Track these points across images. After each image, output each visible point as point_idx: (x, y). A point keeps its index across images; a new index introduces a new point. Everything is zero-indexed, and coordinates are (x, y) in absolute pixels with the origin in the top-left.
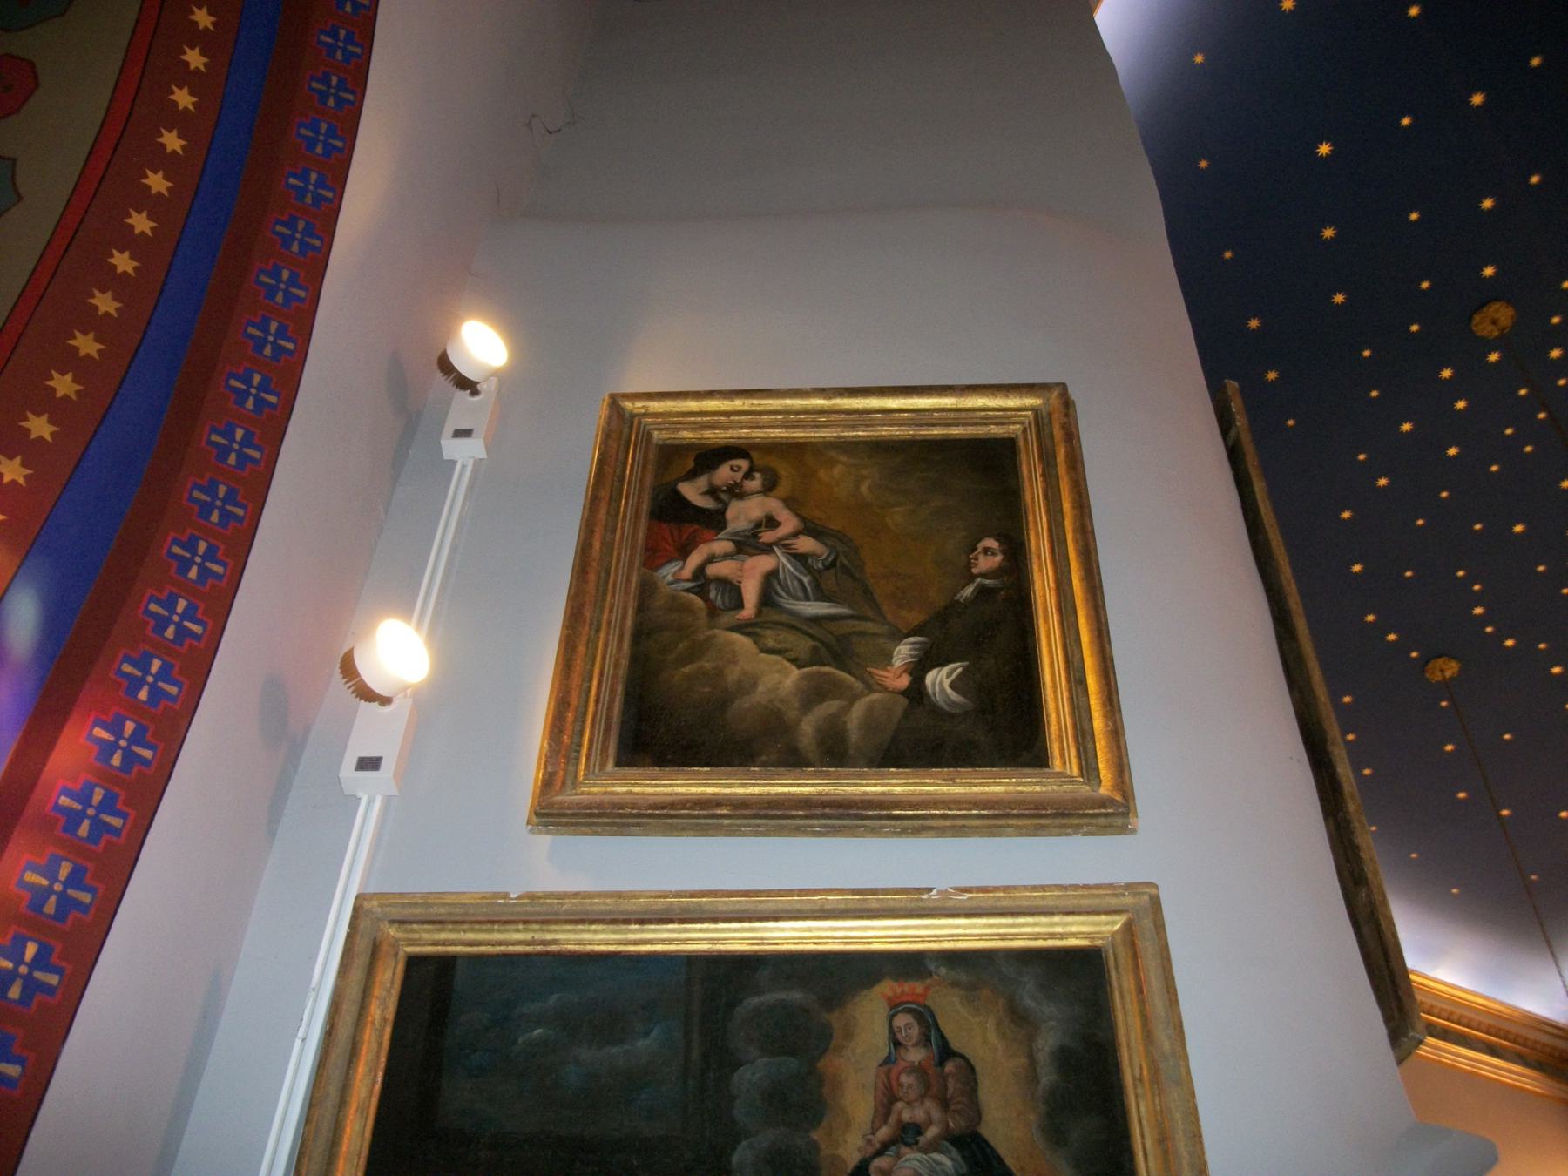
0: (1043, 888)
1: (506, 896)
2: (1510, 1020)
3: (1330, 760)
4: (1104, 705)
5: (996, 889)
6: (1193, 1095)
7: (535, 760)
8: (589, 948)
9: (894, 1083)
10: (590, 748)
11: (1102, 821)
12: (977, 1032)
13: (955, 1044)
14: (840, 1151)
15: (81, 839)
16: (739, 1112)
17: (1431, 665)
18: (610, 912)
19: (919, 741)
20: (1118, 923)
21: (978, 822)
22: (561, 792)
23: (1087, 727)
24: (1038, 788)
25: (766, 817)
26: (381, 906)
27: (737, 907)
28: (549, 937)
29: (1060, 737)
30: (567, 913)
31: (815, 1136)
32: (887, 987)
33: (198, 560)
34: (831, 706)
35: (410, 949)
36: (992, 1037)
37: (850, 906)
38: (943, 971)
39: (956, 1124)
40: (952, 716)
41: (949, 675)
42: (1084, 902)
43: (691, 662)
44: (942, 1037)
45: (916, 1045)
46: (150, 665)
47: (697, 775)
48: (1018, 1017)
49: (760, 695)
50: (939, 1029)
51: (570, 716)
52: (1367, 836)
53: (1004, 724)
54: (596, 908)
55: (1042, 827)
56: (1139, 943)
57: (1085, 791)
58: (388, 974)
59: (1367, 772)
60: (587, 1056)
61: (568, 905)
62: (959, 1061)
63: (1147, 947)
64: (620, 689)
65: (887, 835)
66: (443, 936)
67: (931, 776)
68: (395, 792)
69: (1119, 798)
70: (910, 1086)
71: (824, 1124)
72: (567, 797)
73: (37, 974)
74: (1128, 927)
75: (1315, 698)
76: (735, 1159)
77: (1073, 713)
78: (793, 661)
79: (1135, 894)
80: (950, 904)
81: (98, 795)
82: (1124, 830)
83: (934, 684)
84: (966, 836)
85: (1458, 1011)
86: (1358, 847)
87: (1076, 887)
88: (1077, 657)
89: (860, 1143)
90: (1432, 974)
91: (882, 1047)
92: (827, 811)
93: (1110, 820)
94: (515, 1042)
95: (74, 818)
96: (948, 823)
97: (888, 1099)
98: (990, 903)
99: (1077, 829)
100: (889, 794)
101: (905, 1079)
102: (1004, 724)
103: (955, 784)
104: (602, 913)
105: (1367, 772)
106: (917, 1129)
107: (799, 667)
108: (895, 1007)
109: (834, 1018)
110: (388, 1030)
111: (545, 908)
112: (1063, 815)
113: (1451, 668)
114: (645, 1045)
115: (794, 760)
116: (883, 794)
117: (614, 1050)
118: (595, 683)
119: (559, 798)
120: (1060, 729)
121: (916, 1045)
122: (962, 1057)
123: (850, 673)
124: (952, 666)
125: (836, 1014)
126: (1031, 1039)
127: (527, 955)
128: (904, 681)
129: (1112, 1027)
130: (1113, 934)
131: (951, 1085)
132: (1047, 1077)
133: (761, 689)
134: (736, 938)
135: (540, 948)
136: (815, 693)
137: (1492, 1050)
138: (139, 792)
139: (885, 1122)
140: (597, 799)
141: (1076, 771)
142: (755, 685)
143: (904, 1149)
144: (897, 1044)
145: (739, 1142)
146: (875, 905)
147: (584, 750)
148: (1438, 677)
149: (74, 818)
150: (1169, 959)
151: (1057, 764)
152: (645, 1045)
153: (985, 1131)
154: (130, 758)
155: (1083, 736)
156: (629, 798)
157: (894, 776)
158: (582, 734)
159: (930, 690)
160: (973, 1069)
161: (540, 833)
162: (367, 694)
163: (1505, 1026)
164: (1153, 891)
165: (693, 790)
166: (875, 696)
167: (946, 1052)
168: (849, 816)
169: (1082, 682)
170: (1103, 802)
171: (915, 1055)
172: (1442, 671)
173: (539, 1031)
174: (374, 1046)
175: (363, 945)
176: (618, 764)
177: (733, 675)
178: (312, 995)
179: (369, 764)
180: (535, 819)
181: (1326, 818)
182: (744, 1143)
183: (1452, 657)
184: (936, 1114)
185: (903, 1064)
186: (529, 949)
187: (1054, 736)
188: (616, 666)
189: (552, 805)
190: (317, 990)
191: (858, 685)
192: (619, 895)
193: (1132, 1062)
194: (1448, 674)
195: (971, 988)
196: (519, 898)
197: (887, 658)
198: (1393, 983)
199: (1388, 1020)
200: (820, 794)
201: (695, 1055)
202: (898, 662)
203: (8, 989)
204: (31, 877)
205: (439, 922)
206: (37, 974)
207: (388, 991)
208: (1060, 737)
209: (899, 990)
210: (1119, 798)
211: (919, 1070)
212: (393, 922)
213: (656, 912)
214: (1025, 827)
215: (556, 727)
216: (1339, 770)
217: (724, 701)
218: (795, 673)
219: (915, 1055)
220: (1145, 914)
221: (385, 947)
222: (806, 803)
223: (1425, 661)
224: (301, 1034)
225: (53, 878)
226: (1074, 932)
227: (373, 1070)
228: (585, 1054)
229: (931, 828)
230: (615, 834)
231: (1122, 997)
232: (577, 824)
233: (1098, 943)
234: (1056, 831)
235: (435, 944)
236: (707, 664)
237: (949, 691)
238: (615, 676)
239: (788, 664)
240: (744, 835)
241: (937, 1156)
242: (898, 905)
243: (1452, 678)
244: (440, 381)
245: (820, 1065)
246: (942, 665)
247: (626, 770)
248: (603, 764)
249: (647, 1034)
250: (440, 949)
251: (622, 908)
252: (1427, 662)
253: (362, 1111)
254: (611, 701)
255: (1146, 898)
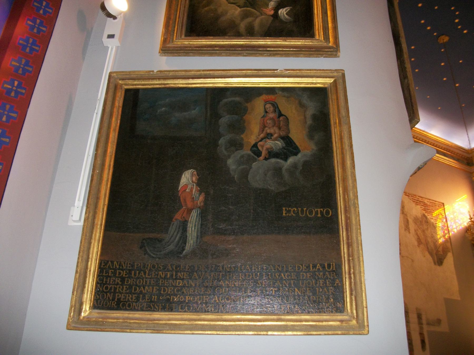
0: (310, 70)
1: (153, 71)
2: (451, 147)
3: (400, 43)
4: (332, 20)
5: (297, 70)
6: (350, 127)
7: (161, 34)
8: (177, 86)
9: (265, 123)
10: (177, 31)
11: (329, 53)
12: (289, 109)
13: (283, 113)
14: (249, 140)
15: (4, 122)
16: (221, 130)
17: (440, 38)
18: (183, 76)
19: (276, 29)
20: (332, 80)
21: (293, 53)
22: (168, 44)
23: (326, 26)
24: (311, 43)
25: (229, 50)
26: (117, 75)
27: (221, 74)
28: (166, 82)
29: (319, 29)
30: (171, 76)
31: (242, 136)
32: (264, 97)
33: (43, 7)
34: (249, 20)
35: (126, 87)
36: (294, 111)
37: (254, 74)
38: (280, 92)
39: (283, 134)
40: (286, 23)
41: (286, 11)
42: (322, 74)
43: (208, 6)
44: (280, 110)
45: (272, 112)
46: (14, 83)
47: (209, 39)
48: (302, 105)
49: (228, 16)
50: (278, 108)
51: (171, 22)
52: (415, 89)
53: (302, 24)
54: (179, 74)
55: (312, 54)
56: (338, 86)
57: (325, 44)
58: (120, 93)
59: (413, 59)
60: (177, 116)
61: (171, 74)
62: (284, 117)
63: (340, 87)
64: (186, 15)
65: (266, 56)
66: (135, 83)
67: (280, 39)
68: (119, 45)
69: (335, 46)
70: (270, 123)
71: (245, 133)
72: (170, 45)
73: (19, 90)
74: (335, 81)
75: (398, 24)
76: (220, 142)
77: (323, 22)
78: (239, 6)
79: (337, 73)
80: (283, 74)
81: (31, 40)
82: (336, 56)
83: (281, 13)
84: (289, 57)
85: (436, 143)
86: (406, 68)
87: (320, 70)
88: (327, 31)
89: (255, 138)
90: (430, 132)
91: (263, 114)
92: (248, 48)
93: (332, 53)
94: (157, 112)
95: (25, 47)
96: (284, 53)
97: (264, 127)
98: (295, 74)
99: (322, 55)
100: (266, 44)
101: (268, 121)
102: (302, 24)
103: (286, 42)
104: (181, 76)
105: (413, 59)
106: (272, 135)
107: (240, 8)
108: (266, 102)
109: (248, 105)
110: (121, 109)
111: (164, 75)
112: (318, 51)
113: (445, 39)
114: (194, 112)
115: (238, 35)
116: (265, 44)
117: (185, 114)
118: (178, 12)
119: (168, 45)
120: (319, 27)
121: (272, 112)
122: (285, 116)
123: (255, 9)
124: (287, 8)
125: (249, 104)
126: (305, 111)
127: (160, 88)
128: (272, 12)
129: (328, 109)
130: (331, 84)
131: (281, 123)
132: (309, 122)
133: (228, 14)
134: (220, 82)
135: (163, 86)
136: (245, 15)
137: (444, 155)
138: (44, 40)
139: (262, 133)
140: (180, 45)
141: (322, 39)
142: (227, 13)
143: (267, 140)
144: (266, 112)
145: (221, 137)
146: (261, 74)
147: (175, 32)
148: (442, 42)
149: (25, 47)
150: (346, 91)
151: (317, 37)
152: (194, 112)
153: (290, 135)
154: (39, 31)
155: (325, 29)
156: (189, 45)
157: (268, 39)
158: (175, 27)
159: (280, 15)
160: (288, 119)
161: (163, 56)
162: (109, 15)
163: (449, 148)
164: (343, 72)
165: (208, 43)
166: (263, 17)
167: (280, 115)
168: (254, 50)
169: (326, 13)
170: (330, 48)
171: (272, 115)
172: (443, 40)
173: (163, 109)
174: (117, 113)
175: (112, 86)
176: (186, 36)
177: (220, 10)
178: (98, 101)
179: (111, 36)
180: (161, 52)
181: (397, 61)
182: (222, 138)
183: (447, 35)
184: (277, 131)
185: (268, 117)
186: (160, 86)
187: (316, 29)
188: (185, 7)
189: (166, 47)
190: (100, 100)
191: (258, 13)
192: (186, 71)
193: (333, 119)
194: (445, 41)
195: (288, 97)
196: (157, 72)
197: (267, 5)
198: (412, 106)
199: (409, 116)
200: (246, 44)
201: (209, 114)
202: (270, 7)
203: (2, 118)
204: (14, 63)
205: (134, 79)
206: (19, 90)
207: (120, 98)
208: (319, 29)
209: (267, 98)
210: (335, 46)
211: (272, 119)
212: (120, 79)
213: (197, 76)
214: (306, 54)
215: (167, 25)
216: (403, 45)
217: (217, 18)
218: (239, 9)
219: (272, 115)
220: (340, 79)
221: (119, 87)
222: (241, 46)
223: (438, 36)
224: (96, 111)
225: (20, 64)
226: (319, 82)
227: (117, 120)
228: (177, 114)
229: (278, 54)
230: (185, 56)
231: (332, 101)
232: (173, 53)
233: (326, 86)
234: (316, 56)
235: (133, 85)
236: (212, 7)
237: (285, 15)
238: (184, 10)
239: (237, 7)
240: (223, 56)
241: (277, 142)
242: (268, 74)
243: (446, 42)
244: (101, 14)
245: (244, 117)
246: (283, 7)
247: (188, 38)
248: (181, 36)
249: (195, 109)
250: (134, 87)
251: (187, 75)
252: (439, 37)
253: (115, 130)
254: (183, 18)
255: (341, 74)
